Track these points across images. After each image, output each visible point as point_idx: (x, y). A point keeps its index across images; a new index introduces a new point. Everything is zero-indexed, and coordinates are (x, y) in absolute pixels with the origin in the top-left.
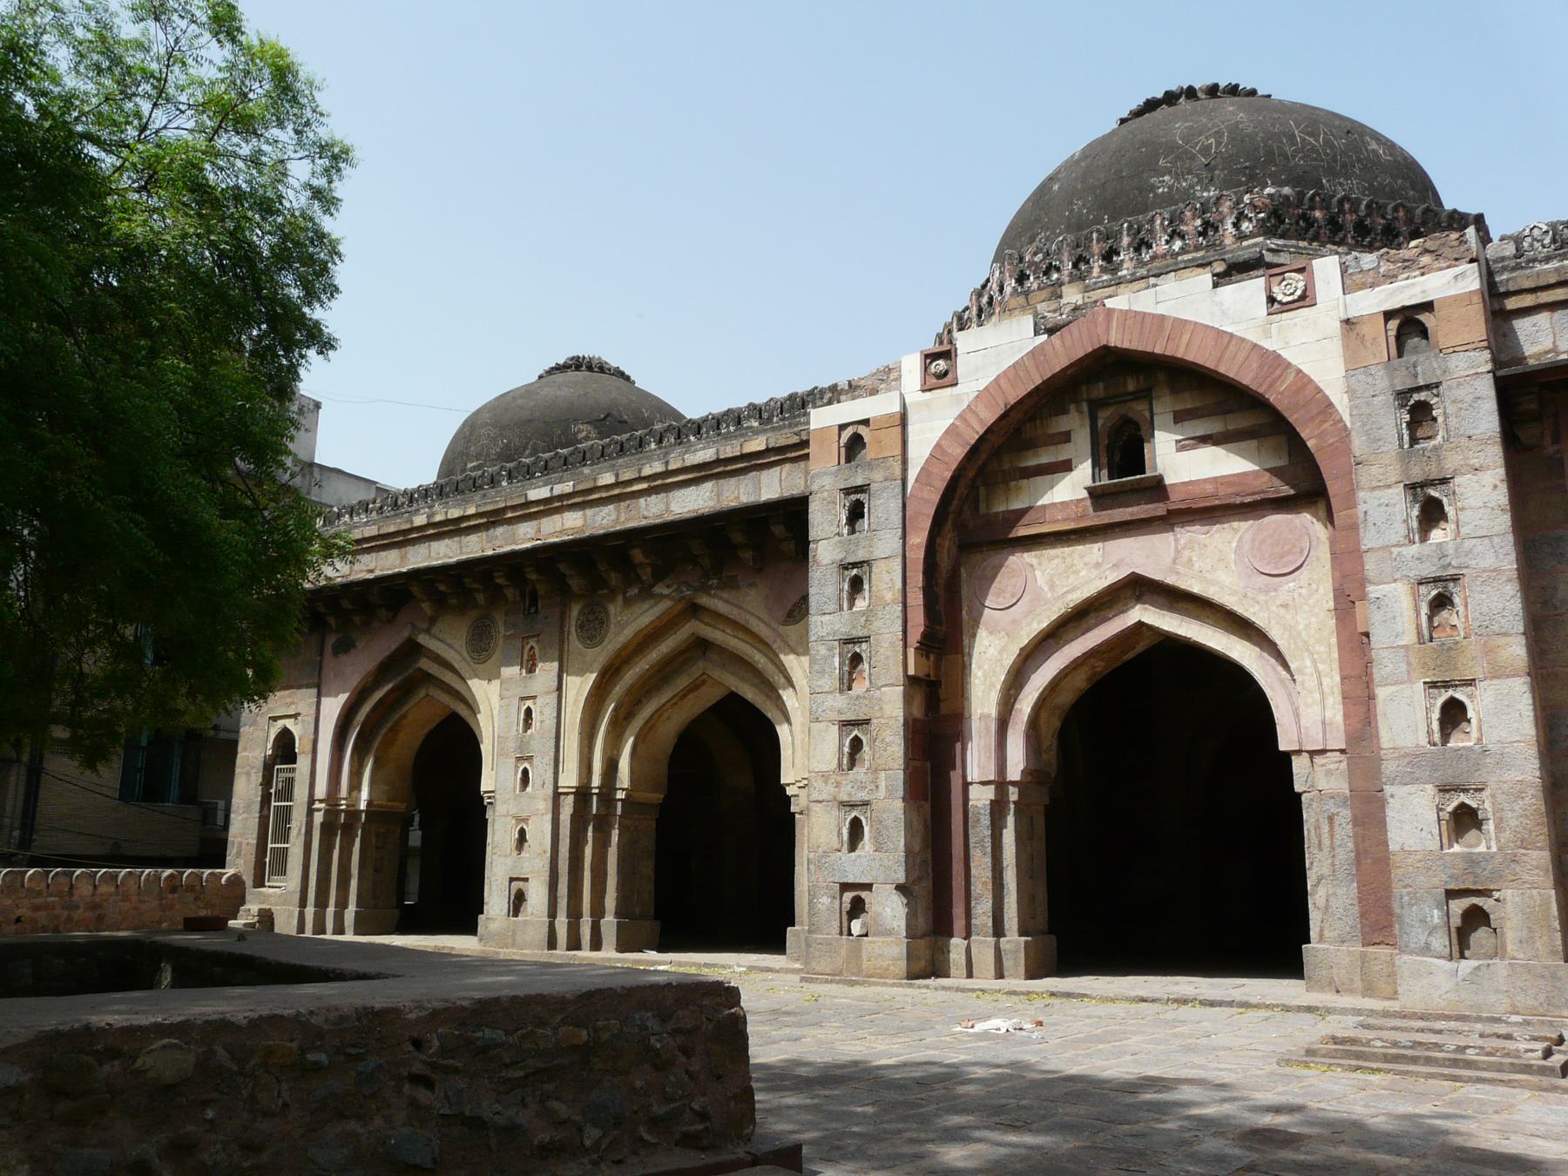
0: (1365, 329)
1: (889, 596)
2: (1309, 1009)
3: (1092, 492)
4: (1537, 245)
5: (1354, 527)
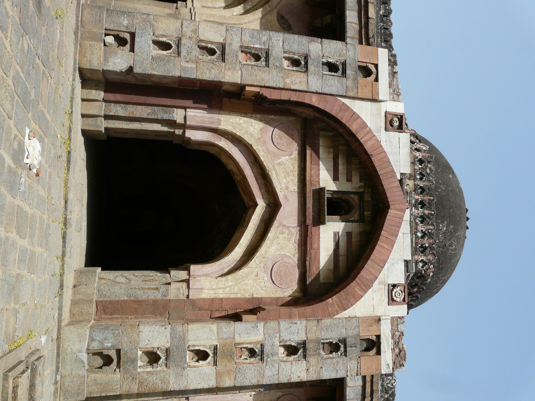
0: (375, 327)
1: (288, 81)
2: (62, 286)
3: (322, 190)
4: (388, 381)
5: (290, 317)
